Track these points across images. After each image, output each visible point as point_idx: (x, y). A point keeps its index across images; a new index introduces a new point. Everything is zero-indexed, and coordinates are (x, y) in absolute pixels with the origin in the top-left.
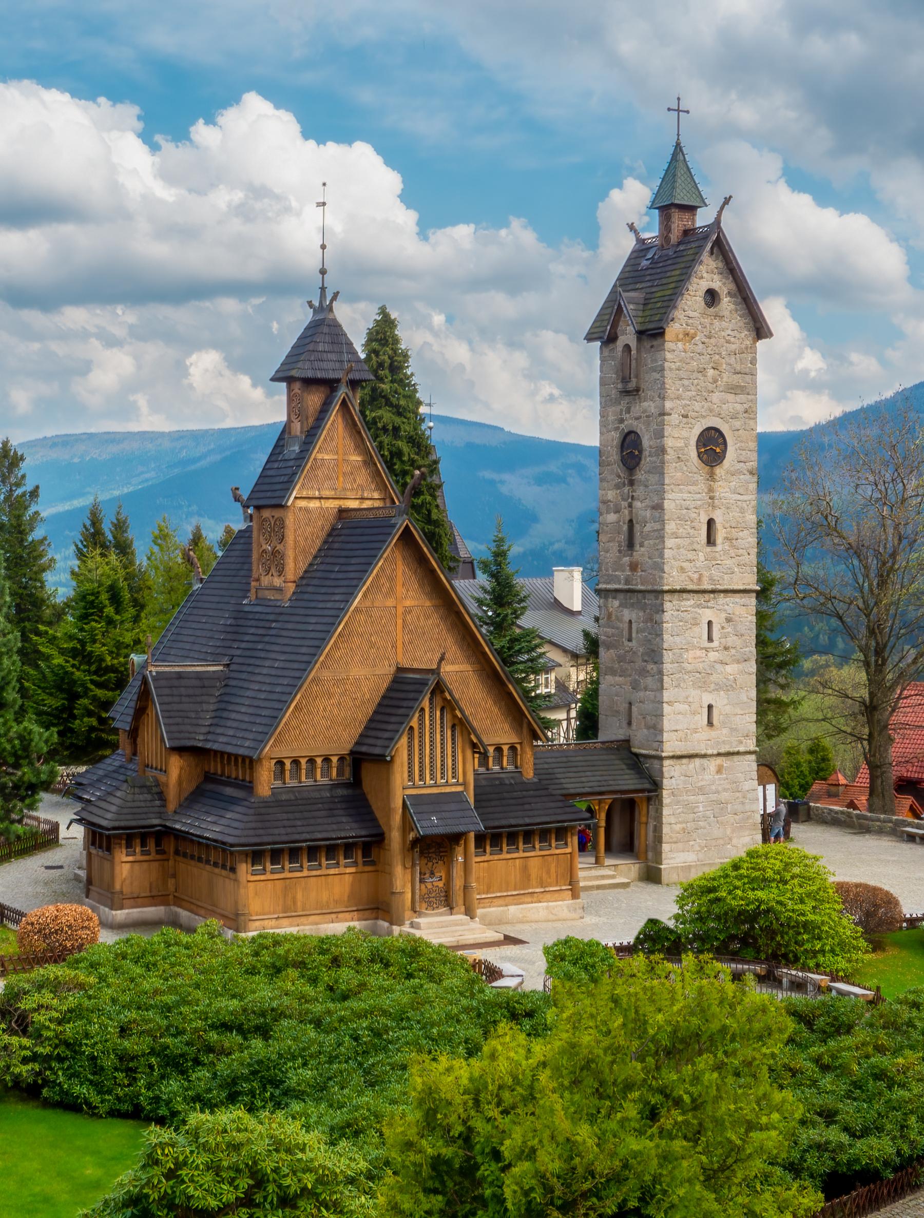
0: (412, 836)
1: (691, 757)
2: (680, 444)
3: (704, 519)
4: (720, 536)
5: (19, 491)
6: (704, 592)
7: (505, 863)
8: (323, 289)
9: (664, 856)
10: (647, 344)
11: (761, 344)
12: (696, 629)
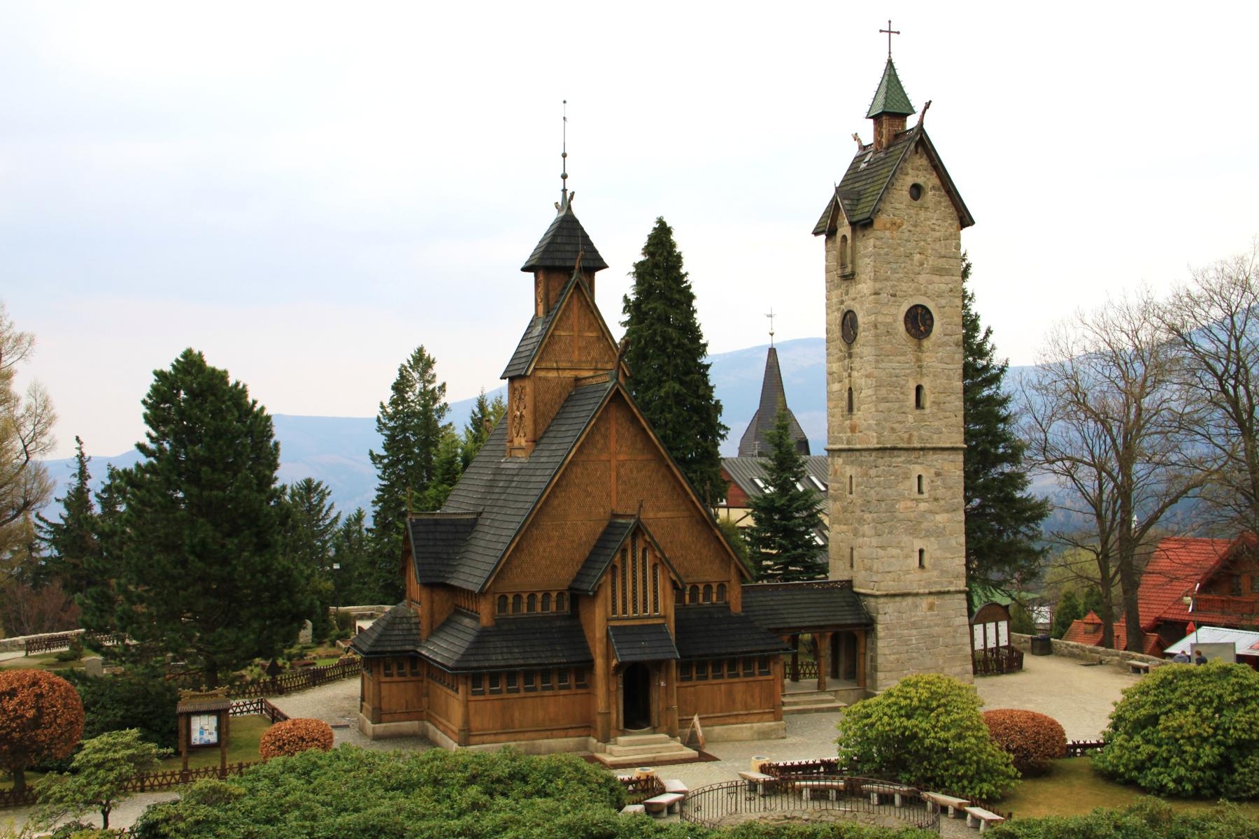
0: (614, 662)
1: (904, 595)
2: (889, 319)
3: (912, 386)
4: (928, 400)
5: (431, 387)
6: (914, 449)
7: (712, 689)
8: (564, 191)
9: (879, 683)
10: (859, 234)
11: (966, 233)
12: (907, 483)
